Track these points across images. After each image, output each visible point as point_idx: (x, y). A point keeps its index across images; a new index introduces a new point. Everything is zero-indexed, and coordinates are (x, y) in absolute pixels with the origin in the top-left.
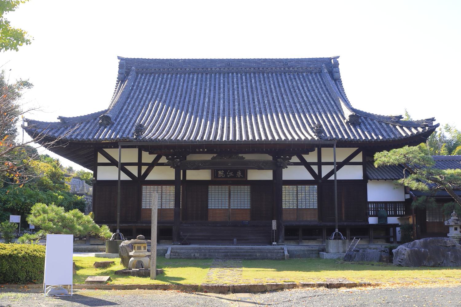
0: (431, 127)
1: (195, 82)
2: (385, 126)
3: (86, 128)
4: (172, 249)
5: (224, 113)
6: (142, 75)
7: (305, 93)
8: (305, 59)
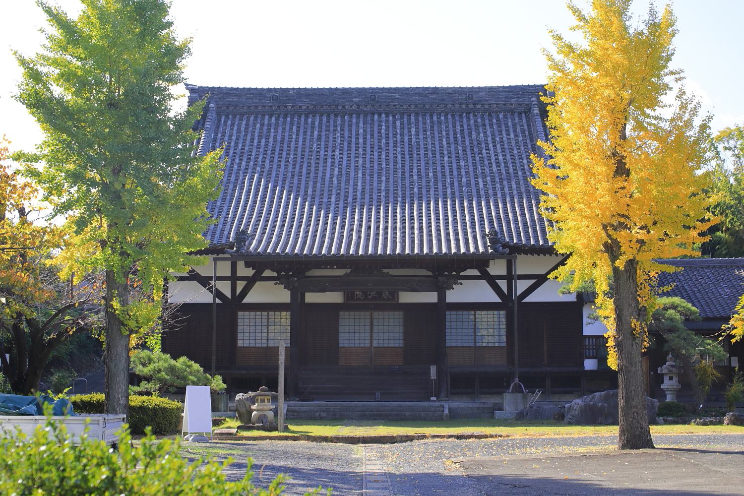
4: (288, 406)
5: (363, 198)
6: (227, 117)
7: (496, 155)
8: (504, 87)
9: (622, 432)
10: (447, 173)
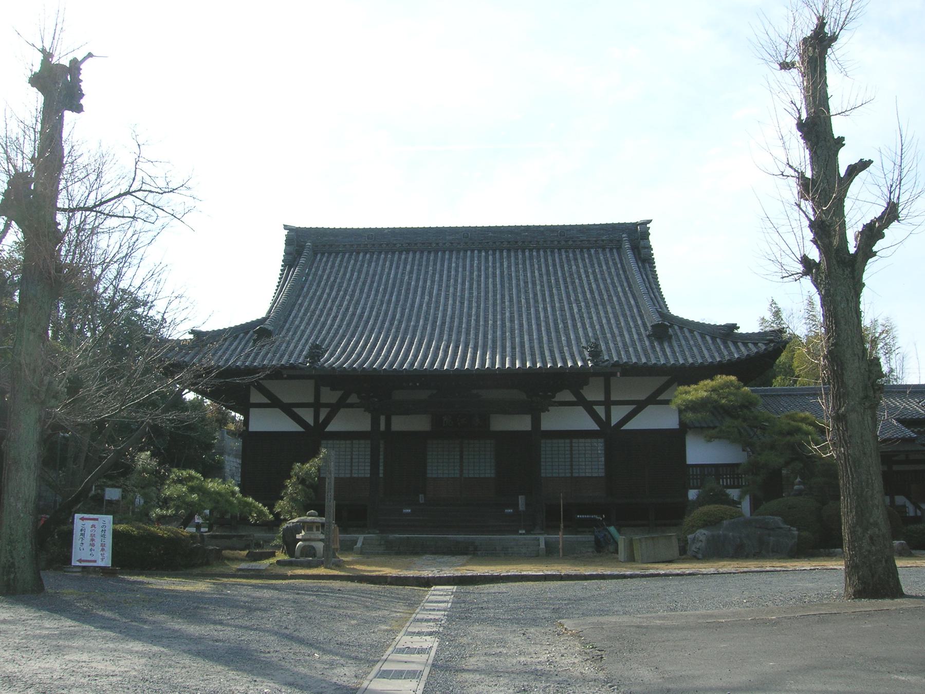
0: (778, 343)
1: (408, 267)
2: (710, 342)
3: (233, 347)
6: (323, 254)
9: (852, 569)
10: (540, 300)
